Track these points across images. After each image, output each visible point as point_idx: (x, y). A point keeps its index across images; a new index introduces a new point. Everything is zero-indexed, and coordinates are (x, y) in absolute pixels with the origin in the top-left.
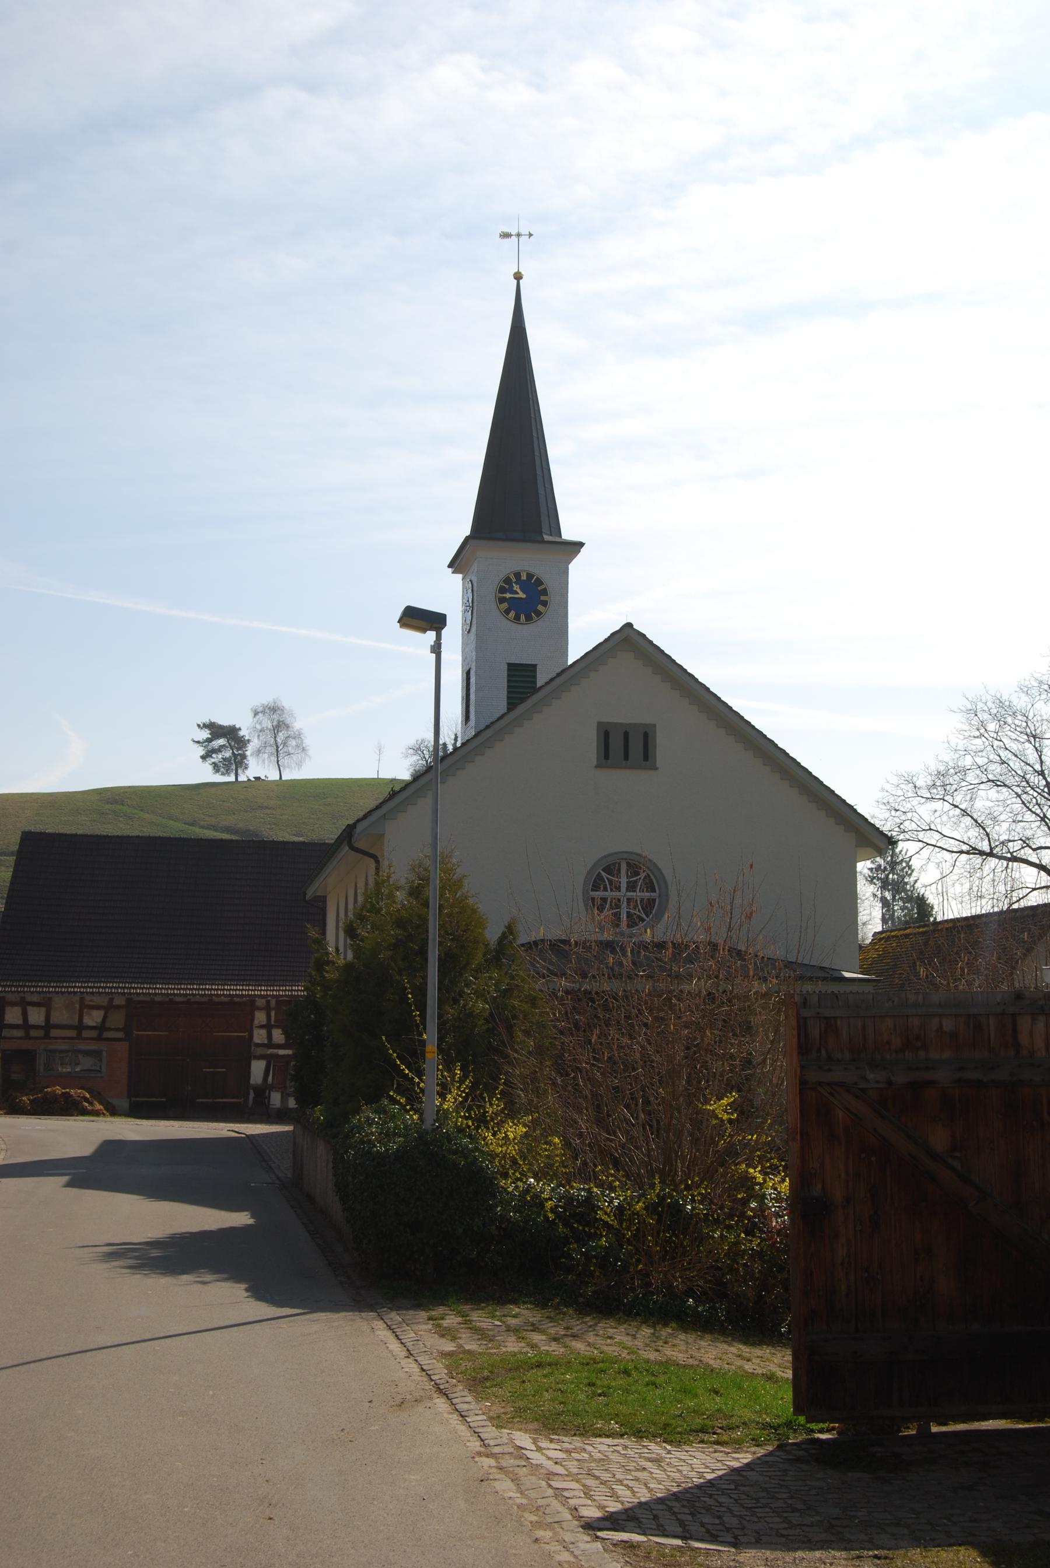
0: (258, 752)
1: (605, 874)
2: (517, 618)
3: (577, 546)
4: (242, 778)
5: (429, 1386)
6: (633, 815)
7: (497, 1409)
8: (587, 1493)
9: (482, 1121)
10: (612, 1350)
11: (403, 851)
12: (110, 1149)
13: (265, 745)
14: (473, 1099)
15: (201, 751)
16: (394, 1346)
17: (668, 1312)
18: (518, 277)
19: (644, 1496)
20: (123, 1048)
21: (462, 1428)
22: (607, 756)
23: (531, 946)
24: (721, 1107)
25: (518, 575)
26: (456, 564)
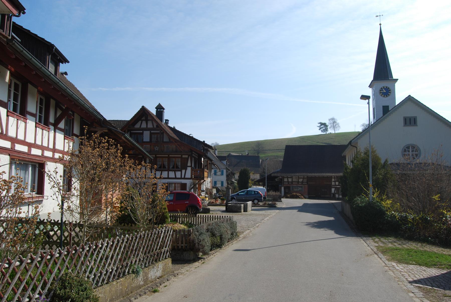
0: (330, 128)
1: (407, 149)
2: (384, 96)
3: (397, 80)
4: (327, 133)
5: (373, 252)
6: (412, 136)
7: (388, 258)
8: (409, 276)
9: (382, 200)
10: (412, 247)
11: (362, 145)
12: (305, 205)
13: (332, 126)
14: (380, 196)
15: (319, 128)
16: (365, 244)
17: (424, 240)
18: (380, 24)
19: (422, 277)
20: (306, 186)
21: (381, 261)
22: (406, 124)
23: (391, 164)
24: (436, 197)
25: (384, 87)
26: (370, 86)
